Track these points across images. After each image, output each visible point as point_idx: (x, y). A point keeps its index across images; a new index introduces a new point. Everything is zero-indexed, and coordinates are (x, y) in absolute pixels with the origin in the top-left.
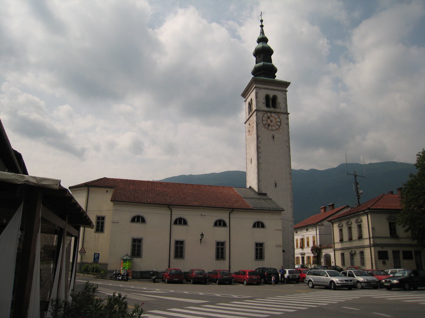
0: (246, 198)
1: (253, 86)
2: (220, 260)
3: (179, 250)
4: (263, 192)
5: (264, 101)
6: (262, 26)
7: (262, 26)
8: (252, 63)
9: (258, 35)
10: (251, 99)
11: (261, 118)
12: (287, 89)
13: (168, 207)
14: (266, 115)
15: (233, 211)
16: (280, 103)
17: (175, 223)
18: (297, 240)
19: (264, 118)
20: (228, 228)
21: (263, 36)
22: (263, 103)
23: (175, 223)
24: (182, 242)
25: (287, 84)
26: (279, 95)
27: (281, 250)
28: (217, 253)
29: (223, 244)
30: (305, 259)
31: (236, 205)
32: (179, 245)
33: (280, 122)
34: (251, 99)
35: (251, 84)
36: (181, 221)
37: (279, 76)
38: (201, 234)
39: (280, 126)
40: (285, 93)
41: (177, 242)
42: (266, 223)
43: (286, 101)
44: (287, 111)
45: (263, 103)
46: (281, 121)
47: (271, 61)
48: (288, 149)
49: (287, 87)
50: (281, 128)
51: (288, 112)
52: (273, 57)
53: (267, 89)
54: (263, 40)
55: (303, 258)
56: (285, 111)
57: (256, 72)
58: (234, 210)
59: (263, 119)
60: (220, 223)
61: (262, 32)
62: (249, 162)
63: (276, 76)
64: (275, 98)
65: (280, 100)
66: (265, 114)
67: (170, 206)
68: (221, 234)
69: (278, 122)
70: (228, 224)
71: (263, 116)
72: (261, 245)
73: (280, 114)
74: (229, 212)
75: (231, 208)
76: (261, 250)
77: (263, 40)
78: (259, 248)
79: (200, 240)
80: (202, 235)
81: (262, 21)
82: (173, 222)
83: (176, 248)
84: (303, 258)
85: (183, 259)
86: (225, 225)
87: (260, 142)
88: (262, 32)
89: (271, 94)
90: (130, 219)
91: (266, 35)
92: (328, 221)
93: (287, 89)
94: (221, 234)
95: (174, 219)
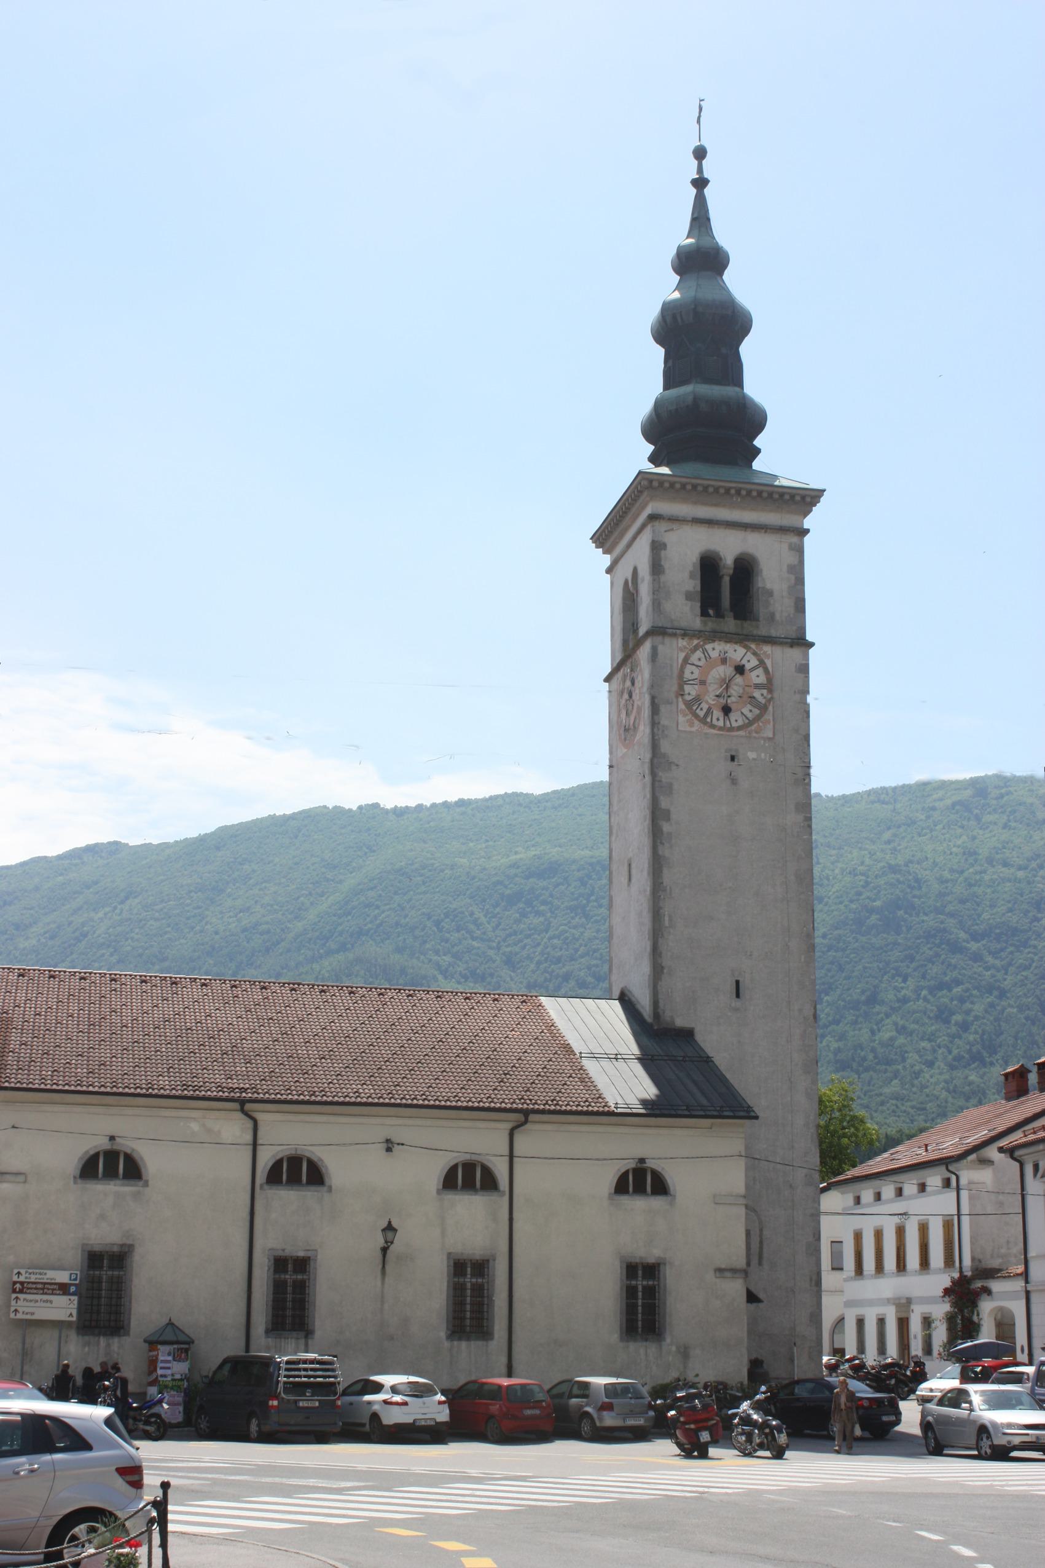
0: (593, 1056)
1: (643, 508)
2: (468, 1339)
3: (289, 1297)
4: (680, 1022)
5: (694, 585)
6: (700, 183)
7: (700, 183)
8: (641, 377)
9: (679, 235)
10: (635, 571)
11: (676, 672)
12: (807, 523)
13: (243, 1111)
14: (699, 653)
15: (526, 1122)
16: (770, 593)
17: (274, 1176)
18: (836, 1243)
19: (689, 669)
20: (506, 1198)
21: (705, 242)
22: (689, 596)
23: (274, 1176)
24: (302, 1264)
25: (806, 499)
26: (767, 552)
27: (736, 1288)
28: (630, 1311)
29: (481, 1267)
30: (916, 1326)
31: (540, 1098)
32: (289, 1277)
33: (769, 686)
34: (635, 571)
35: (635, 500)
36: (299, 1172)
37: (777, 457)
38: (385, 1224)
39: (763, 709)
40: (795, 539)
41: (280, 1263)
42: (673, 1176)
43: (800, 581)
44: (802, 629)
45: (689, 596)
46: (770, 680)
47: (733, 372)
48: (800, 818)
49: (805, 515)
50: (769, 716)
51: (809, 637)
52: (748, 349)
53: (710, 522)
54: (701, 260)
55: (903, 1324)
56: (791, 631)
57: (666, 431)
58: (532, 1117)
59: (687, 675)
60: (467, 1177)
61: (700, 219)
62: (621, 878)
63: (757, 451)
64: (745, 569)
65: (770, 576)
66: (696, 649)
67: (248, 1106)
68: (471, 1223)
69: (758, 686)
70: (503, 1183)
71: (686, 661)
72: (652, 1270)
73: (767, 649)
74: (509, 1126)
75: (516, 1111)
76: (651, 1293)
77: (701, 260)
78: (640, 1283)
79: (379, 1254)
80: (390, 1228)
81: (700, 154)
82: (261, 1177)
83: (278, 1287)
84: (903, 1324)
85: (449, 1254)
86: (489, 1183)
87: (669, 789)
88: (700, 219)
89: (729, 547)
90: (72, 1163)
91: (723, 234)
92: (1001, 1150)
93: (807, 523)
94: (471, 1223)
95: (266, 1159)
